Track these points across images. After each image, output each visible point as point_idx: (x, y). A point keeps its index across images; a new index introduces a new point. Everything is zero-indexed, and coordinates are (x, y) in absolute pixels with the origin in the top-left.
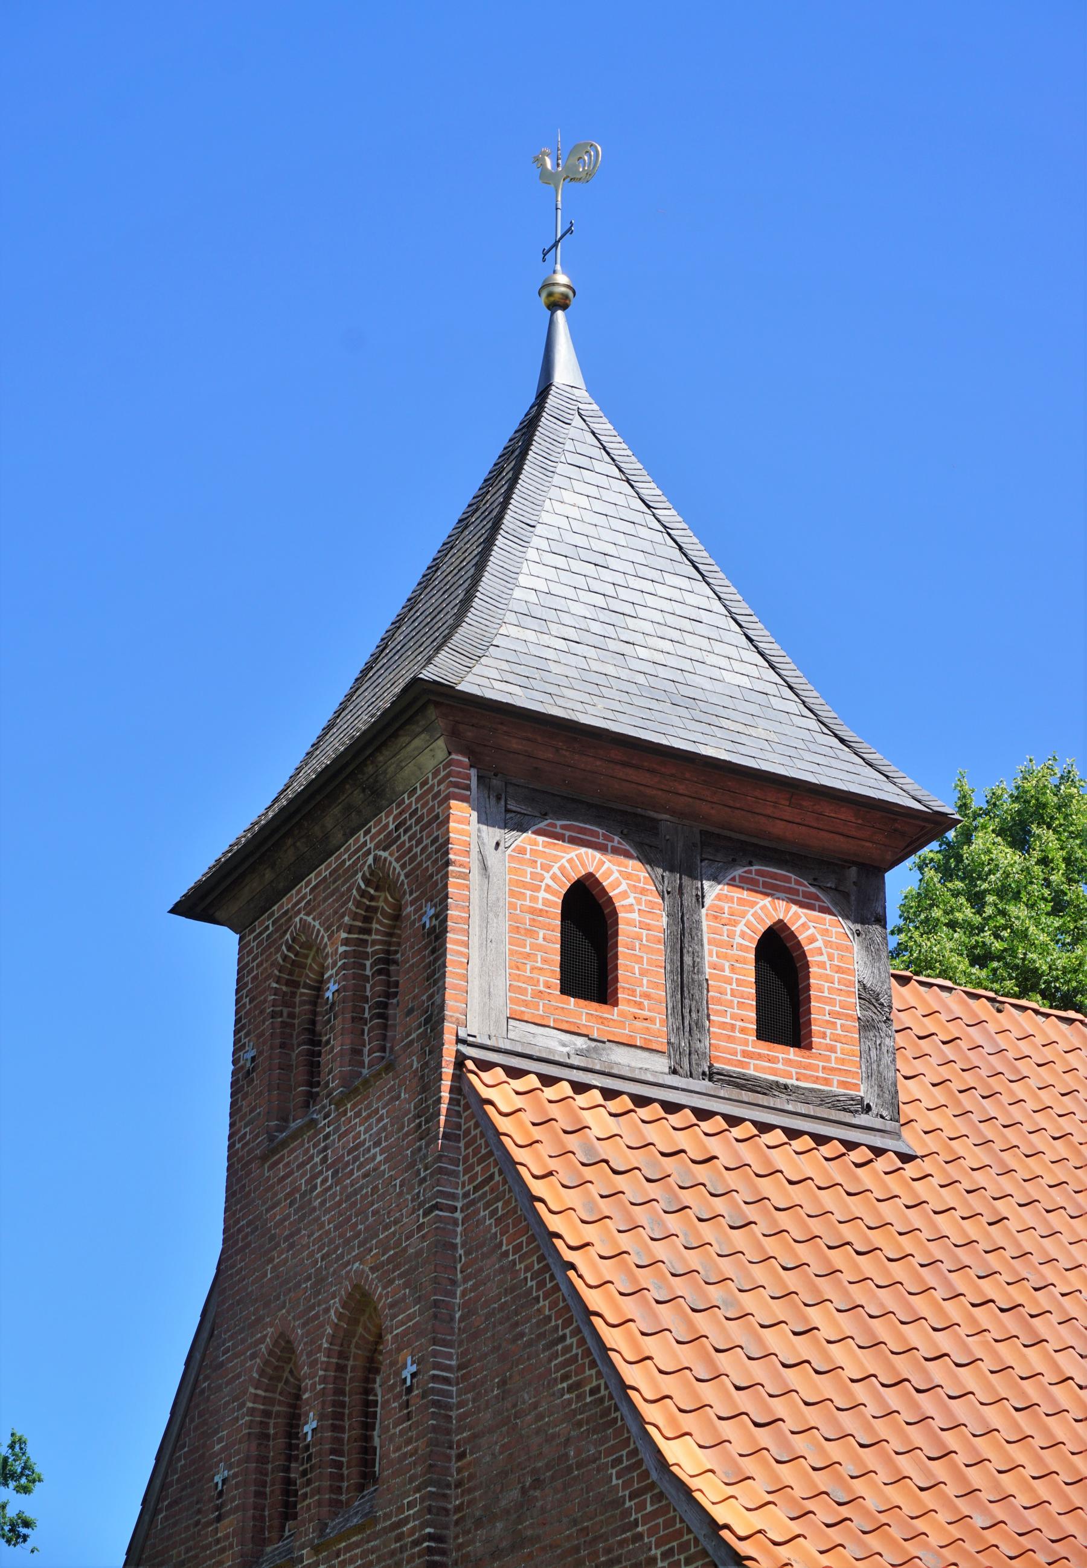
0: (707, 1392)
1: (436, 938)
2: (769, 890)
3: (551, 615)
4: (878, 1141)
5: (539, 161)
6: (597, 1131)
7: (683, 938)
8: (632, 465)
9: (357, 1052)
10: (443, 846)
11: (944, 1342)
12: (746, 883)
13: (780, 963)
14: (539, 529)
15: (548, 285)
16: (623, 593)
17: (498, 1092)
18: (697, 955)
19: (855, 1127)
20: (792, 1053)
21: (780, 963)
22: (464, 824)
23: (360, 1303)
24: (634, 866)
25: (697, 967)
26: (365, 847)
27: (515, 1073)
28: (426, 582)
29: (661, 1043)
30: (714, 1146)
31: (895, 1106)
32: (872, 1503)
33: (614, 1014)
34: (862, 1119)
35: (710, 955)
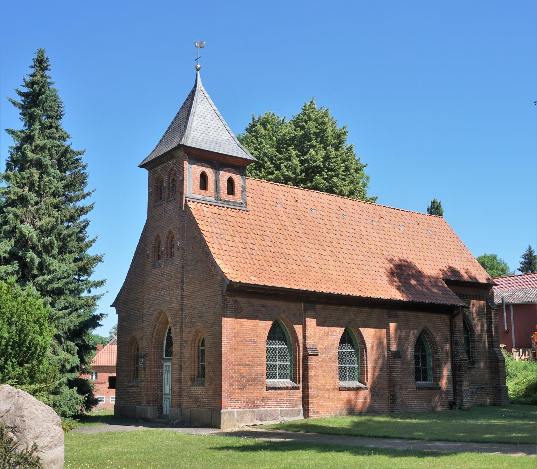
0: (221, 251)
1: (182, 181)
3: (198, 129)
4: (243, 209)
5: (195, 43)
6: (205, 211)
7: (217, 180)
8: (210, 99)
9: (169, 194)
10: (183, 168)
11: (252, 241)
13: (231, 182)
14: (196, 113)
15: (196, 67)
16: (209, 124)
17: (191, 205)
18: (219, 182)
19: (241, 207)
20: (232, 196)
21: (231, 182)
22: (186, 165)
23: (170, 232)
25: (219, 184)
26: (170, 164)
27: (193, 202)
28: (177, 116)
29: (213, 196)
30: (221, 212)
31: (246, 203)
32: (242, 267)
33: (207, 192)
34: (242, 205)
35: (221, 182)
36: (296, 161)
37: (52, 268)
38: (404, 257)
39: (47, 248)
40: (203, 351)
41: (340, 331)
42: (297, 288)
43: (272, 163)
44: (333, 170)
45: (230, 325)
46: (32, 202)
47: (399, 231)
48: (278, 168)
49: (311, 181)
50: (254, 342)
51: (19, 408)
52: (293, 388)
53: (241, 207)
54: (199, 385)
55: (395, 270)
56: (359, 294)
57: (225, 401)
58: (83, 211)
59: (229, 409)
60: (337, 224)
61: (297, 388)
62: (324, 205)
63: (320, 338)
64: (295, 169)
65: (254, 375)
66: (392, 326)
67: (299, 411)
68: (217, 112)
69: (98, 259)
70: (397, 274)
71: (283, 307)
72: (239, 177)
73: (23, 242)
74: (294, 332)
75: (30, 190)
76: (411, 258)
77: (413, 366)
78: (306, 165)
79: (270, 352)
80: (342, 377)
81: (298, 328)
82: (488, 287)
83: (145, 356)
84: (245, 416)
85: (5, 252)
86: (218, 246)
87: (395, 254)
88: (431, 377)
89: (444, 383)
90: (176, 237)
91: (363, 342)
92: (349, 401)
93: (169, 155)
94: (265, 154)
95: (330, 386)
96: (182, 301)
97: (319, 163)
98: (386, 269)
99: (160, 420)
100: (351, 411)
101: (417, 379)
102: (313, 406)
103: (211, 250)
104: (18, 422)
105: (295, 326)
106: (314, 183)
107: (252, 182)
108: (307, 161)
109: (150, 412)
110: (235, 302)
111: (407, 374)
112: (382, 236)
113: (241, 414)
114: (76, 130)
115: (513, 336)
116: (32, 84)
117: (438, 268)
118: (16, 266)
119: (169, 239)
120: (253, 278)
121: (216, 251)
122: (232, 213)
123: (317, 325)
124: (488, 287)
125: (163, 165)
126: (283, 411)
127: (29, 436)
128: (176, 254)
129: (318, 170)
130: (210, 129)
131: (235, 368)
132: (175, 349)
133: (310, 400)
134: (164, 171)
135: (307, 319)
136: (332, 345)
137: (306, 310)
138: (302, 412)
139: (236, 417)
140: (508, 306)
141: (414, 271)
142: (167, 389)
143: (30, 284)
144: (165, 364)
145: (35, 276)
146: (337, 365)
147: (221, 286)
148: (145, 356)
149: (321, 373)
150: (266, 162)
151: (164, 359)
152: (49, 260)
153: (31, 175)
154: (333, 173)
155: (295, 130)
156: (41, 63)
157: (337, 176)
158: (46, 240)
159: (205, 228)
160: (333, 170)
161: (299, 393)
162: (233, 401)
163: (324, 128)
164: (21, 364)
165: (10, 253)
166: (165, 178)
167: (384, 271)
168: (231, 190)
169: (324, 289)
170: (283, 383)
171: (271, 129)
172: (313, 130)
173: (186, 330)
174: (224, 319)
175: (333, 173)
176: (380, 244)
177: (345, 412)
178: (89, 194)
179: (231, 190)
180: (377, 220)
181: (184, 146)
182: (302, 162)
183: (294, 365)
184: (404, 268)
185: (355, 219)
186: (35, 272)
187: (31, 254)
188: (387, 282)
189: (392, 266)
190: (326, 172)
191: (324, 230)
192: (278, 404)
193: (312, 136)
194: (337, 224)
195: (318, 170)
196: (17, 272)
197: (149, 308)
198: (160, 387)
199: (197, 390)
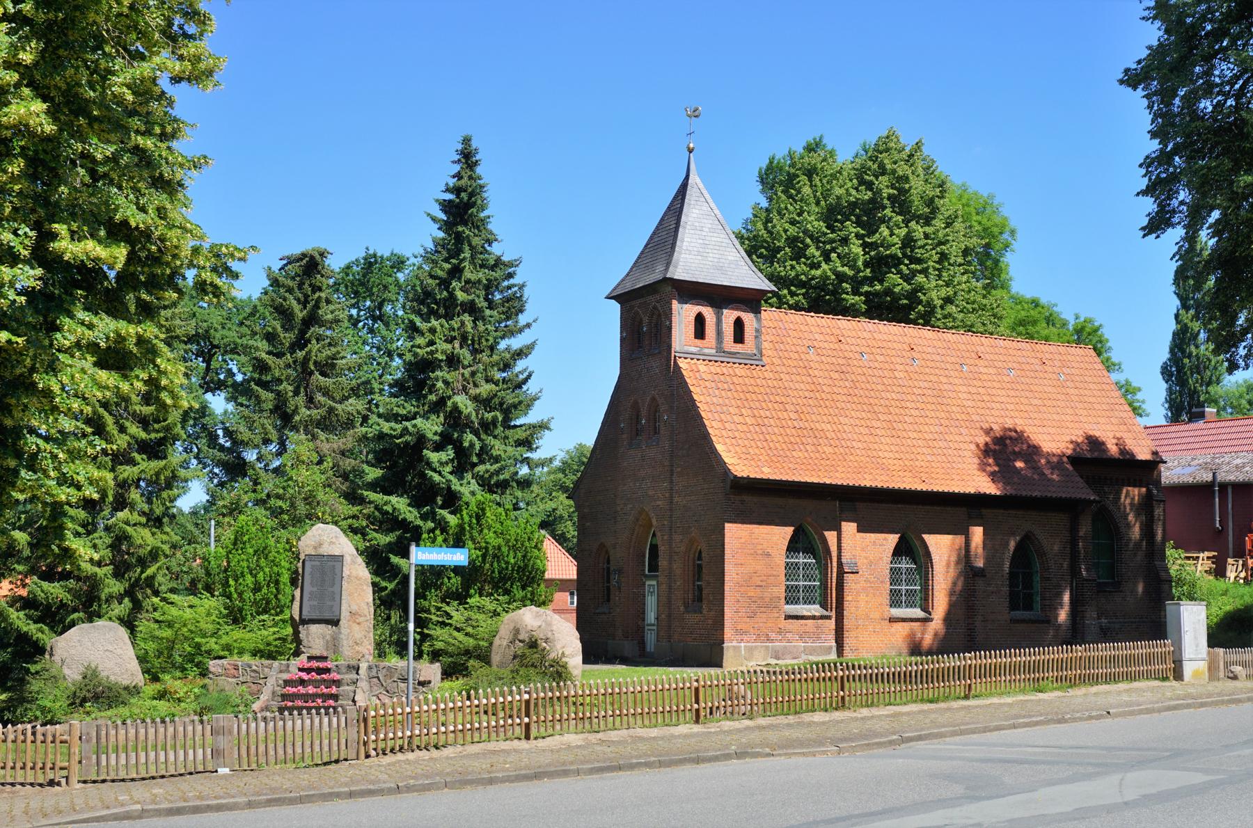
1: (670, 328)
2: (737, 309)
12: (733, 309)
13: (739, 324)
17: (682, 364)
19: (755, 359)
21: (739, 324)
22: (675, 305)
23: (653, 399)
24: (709, 309)
26: (652, 299)
35: (724, 326)
36: (856, 249)
37: (494, 453)
38: (1009, 423)
39: (487, 427)
40: (700, 566)
41: (893, 539)
42: (828, 482)
43: (818, 248)
44: (919, 261)
45: (736, 535)
46: (466, 363)
47: (1006, 379)
48: (827, 259)
49: (881, 282)
50: (768, 555)
51: (549, 624)
52: (822, 617)
53: (755, 359)
54: (695, 612)
55: (992, 447)
56: (924, 487)
57: (728, 632)
58: (520, 354)
59: (734, 644)
60: (902, 375)
61: (828, 618)
62: (885, 344)
63: (863, 550)
64: (855, 260)
65: (767, 600)
66: (977, 533)
67: (831, 647)
68: (720, 216)
69: (543, 426)
70: (995, 451)
71: (809, 510)
72: (751, 315)
73: (455, 420)
74: (824, 541)
75: (461, 347)
76: (1021, 423)
77: (1006, 589)
78: (872, 253)
79: (791, 569)
80: (895, 601)
81: (831, 536)
82: (1153, 465)
83: (620, 571)
84: (756, 653)
85: (436, 433)
86: (720, 425)
87: (991, 419)
88: (1037, 606)
89: (1063, 615)
90: (662, 408)
91: (928, 554)
92: (912, 636)
93: (652, 288)
94: (806, 232)
95: (876, 615)
96: (671, 497)
97: (896, 250)
98: (978, 446)
99: (641, 658)
100: (915, 649)
101: (1013, 606)
102: (849, 642)
103: (710, 431)
104: (549, 635)
105: (826, 533)
106: (886, 284)
107: (770, 315)
108: (873, 246)
109: (628, 648)
110: (742, 502)
111: (996, 603)
112: (973, 390)
113: (750, 650)
114: (508, 229)
115: (1231, 538)
116: (457, 190)
117: (1068, 439)
118: (450, 453)
119: (650, 404)
120: (766, 470)
121: (717, 432)
122: (740, 370)
123: (859, 531)
124: (1153, 465)
125: (642, 300)
126: (808, 644)
127: (559, 646)
128: (663, 428)
129: (894, 262)
130: (710, 252)
131: (742, 589)
132: (663, 562)
133: (846, 634)
134: (645, 309)
135: (843, 524)
136: (881, 558)
137: (842, 510)
138: (834, 649)
139: (743, 653)
140: (1224, 486)
141: (1025, 446)
142: (651, 617)
143: (468, 476)
144: (648, 583)
145: (475, 465)
146: (888, 587)
147: (724, 481)
148: (620, 571)
149: (863, 597)
150: (808, 246)
151: (646, 576)
152: (490, 440)
153: (463, 323)
154: (918, 267)
155: (857, 189)
156: (468, 158)
157: (925, 272)
158: (486, 415)
159: (702, 398)
160: (919, 261)
161: (831, 624)
162: (740, 632)
163: (907, 186)
164: (523, 588)
165: (441, 434)
166: (646, 320)
167: (973, 447)
168: (739, 337)
169: (867, 481)
170: (809, 610)
171: (819, 184)
172: (886, 192)
173: (677, 538)
174: (727, 525)
175: (918, 267)
176: (969, 403)
177: (905, 651)
178: (528, 326)
179: (739, 337)
180: (972, 362)
181: (671, 279)
182: (865, 245)
183: (824, 586)
184: (1008, 442)
185: (933, 364)
186: (475, 459)
187: (469, 438)
188: (975, 466)
189: (988, 439)
190: (906, 265)
191: (879, 387)
192: (801, 637)
193: (885, 201)
194: (902, 375)
195: (894, 262)
196: (452, 460)
197: (625, 505)
198: (642, 613)
199: (692, 619)
